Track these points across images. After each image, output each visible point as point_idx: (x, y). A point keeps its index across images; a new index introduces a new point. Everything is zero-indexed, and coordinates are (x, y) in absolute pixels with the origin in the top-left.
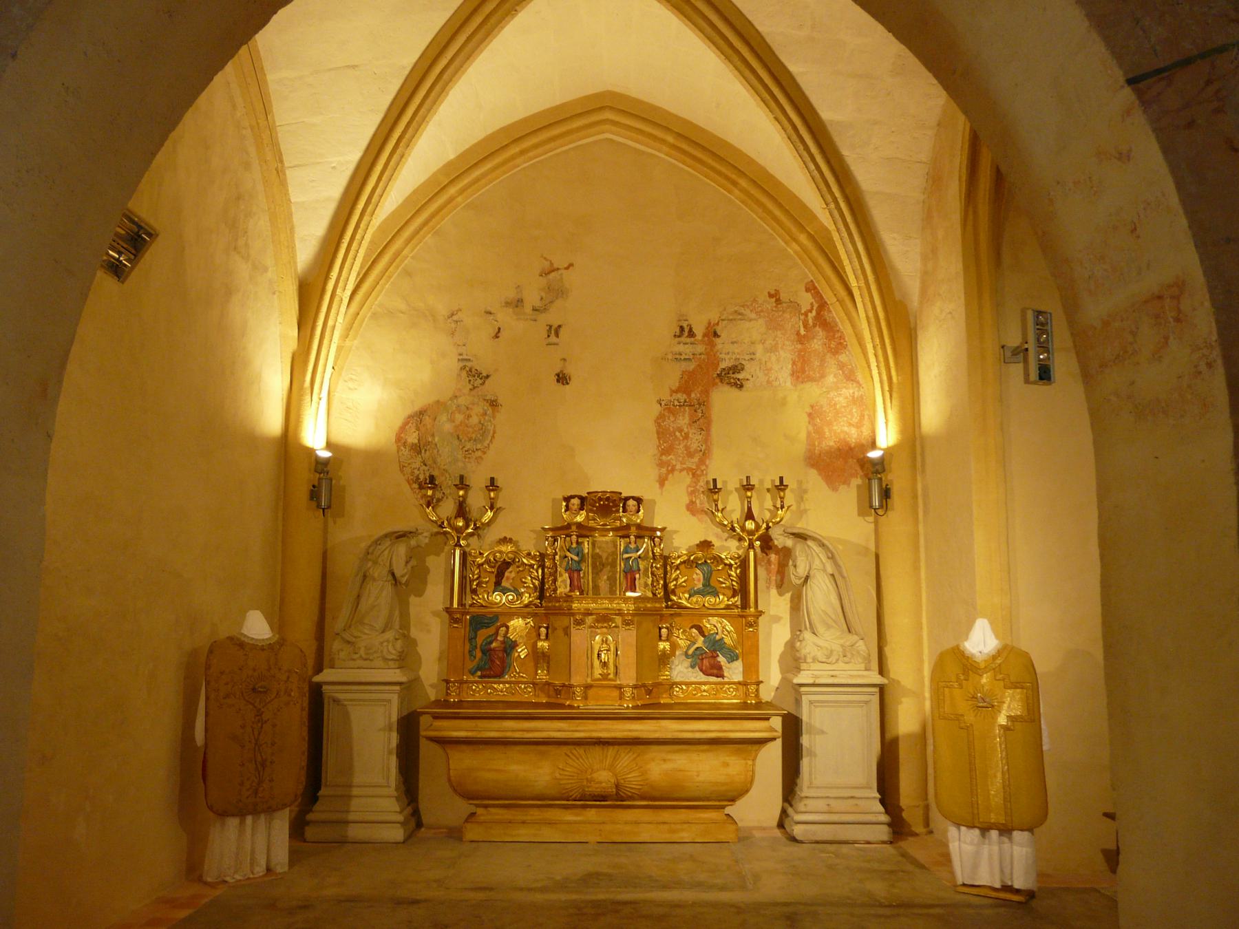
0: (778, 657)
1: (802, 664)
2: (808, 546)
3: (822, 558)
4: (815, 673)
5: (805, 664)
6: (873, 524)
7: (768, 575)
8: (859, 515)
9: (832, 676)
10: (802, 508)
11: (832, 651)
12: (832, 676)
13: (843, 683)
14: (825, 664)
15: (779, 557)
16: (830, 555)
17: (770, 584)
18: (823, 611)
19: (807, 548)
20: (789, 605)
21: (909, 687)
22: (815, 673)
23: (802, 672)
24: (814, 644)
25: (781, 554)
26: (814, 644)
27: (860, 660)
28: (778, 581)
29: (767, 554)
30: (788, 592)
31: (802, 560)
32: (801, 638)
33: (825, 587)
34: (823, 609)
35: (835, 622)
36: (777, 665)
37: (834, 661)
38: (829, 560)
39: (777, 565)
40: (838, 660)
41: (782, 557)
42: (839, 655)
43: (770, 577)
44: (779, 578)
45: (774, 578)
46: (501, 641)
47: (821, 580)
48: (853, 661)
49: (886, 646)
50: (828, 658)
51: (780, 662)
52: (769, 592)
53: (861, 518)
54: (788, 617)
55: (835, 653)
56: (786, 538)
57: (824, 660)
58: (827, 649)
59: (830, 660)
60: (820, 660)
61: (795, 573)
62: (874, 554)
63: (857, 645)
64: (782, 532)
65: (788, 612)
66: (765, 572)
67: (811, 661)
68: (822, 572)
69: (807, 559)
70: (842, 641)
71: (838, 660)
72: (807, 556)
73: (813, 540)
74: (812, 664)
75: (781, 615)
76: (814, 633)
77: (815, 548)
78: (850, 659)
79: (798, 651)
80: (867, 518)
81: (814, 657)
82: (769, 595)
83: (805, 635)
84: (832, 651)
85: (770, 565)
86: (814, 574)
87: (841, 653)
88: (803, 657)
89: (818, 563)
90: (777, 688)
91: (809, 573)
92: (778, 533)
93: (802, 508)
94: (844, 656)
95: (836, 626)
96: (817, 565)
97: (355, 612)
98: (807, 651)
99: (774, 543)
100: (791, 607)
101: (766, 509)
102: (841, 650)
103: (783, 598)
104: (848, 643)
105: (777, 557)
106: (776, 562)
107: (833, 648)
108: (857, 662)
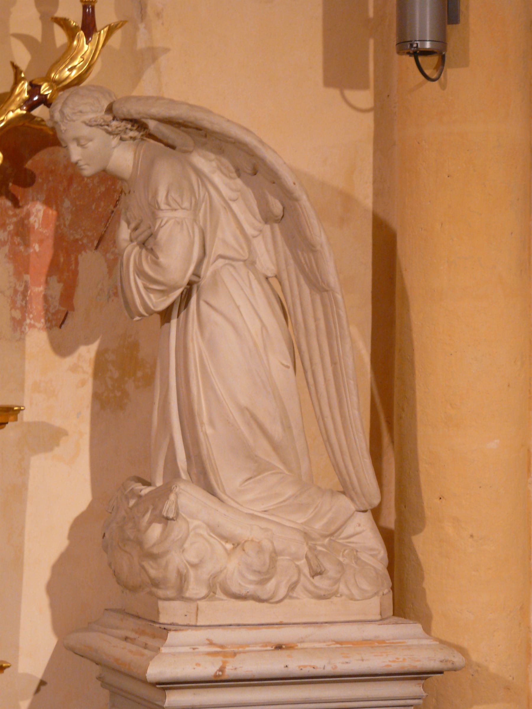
0: (45, 575)
1: (161, 604)
2: (199, 173)
3: (242, 217)
4: (218, 635)
5: (177, 604)
6: (371, 115)
7: (18, 274)
8: (328, 82)
9: (279, 647)
10: (141, 44)
11: (275, 554)
12: (279, 647)
13: (319, 671)
14: (251, 603)
15: (59, 216)
16: (277, 207)
17: (24, 310)
18: (243, 410)
19: (194, 178)
20: (87, 391)
21: (493, 668)
22: (218, 635)
23: (172, 637)
24: (213, 529)
25: (67, 203)
26: (213, 529)
27: (365, 586)
28: (55, 304)
29: (16, 203)
30: (88, 342)
31: (179, 223)
32: (168, 510)
33: (254, 327)
34: (244, 401)
35: (276, 447)
36: (44, 600)
37: (282, 592)
38: (267, 228)
39: (50, 242)
40: (292, 587)
41: (68, 217)
42: (300, 571)
43: (26, 288)
44: (57, 288)
45: (39, 289)
46: (23, 104)
47: (241, 302)
48: (342, 588)
49: (417, 531)
50: (262, 582)
51: (50, 588)
52: (22, 340)
53: (334, 93)
54: (86, 428)
55: (283, 561)
56: (115, 141)
57: (251, 588)
58: (260, 550)
59: (271, 585)
60: (235, 589)
61: (147, 268)
62: (370, 217)
63: (349, 530)
64: (100, 115)
65: (87, 414)
66: (11, 267)
67: (203, 592)
68: (243, 271)
69: (195, 220)
70: (300, 519)
71: (292, 587)
72: (195, 209)
73: (220, 151)
74: (202, 604)
75: (58, 423)
76: (211, 492)
77: (217, 178)
78: (337, 581)
79: (153, 557)
80: (350, 94)
81: (214, 576)
82: (23, 350)
83: (183, 500)
84: (275, 554)
85: (27, 245)
86: (215, 274)
87: (302, 563)
88: (172, 576)
89: (231, 240)
90: (42, 683)
91: (196, 274)
92: (87, 117)
93: (141, 44)
94: (315, 574)
95: (281, 466)
96: (225, 242)
97: (328, 441)
98: (191, 556)
99: (68, 157)
100: (96, 396)
101: (18, 36)
102: (305, 549)
103: (70, 360)
104: (318, 526)
105: (52, 213)
106: (49, 232)
107: (279, 546)
108: (355, 592)
